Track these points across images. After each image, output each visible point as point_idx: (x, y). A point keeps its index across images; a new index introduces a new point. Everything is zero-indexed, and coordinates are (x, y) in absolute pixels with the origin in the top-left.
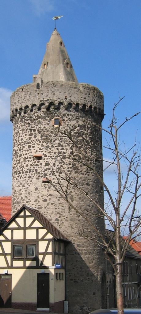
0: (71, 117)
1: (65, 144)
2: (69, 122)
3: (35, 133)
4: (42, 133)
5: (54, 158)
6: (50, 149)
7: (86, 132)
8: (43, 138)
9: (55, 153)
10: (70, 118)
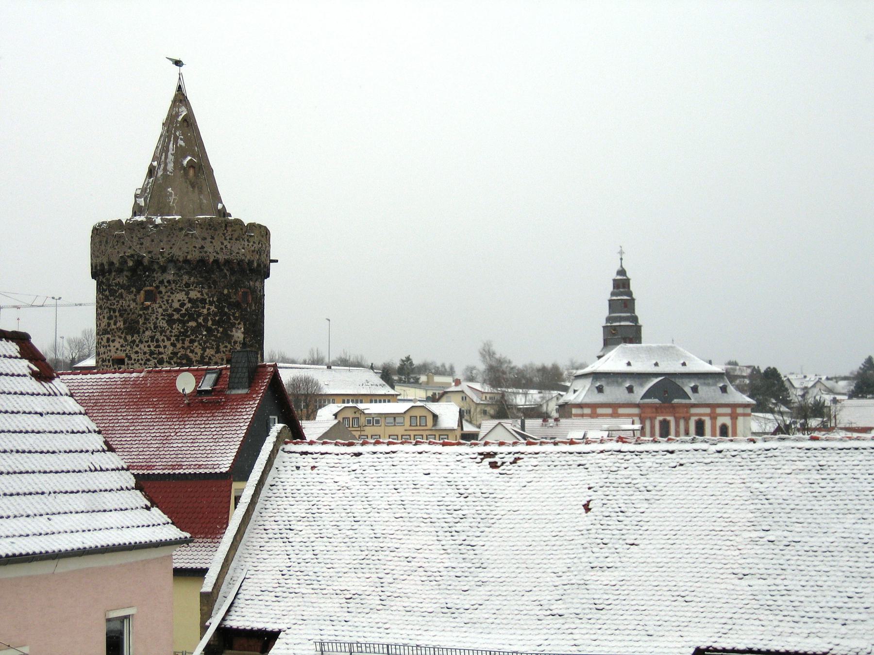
1: (162, 337)
3: (116, 317)
4: (125, 316)
5: (143, 362)
6: (137, 346)
9: (145, 353)
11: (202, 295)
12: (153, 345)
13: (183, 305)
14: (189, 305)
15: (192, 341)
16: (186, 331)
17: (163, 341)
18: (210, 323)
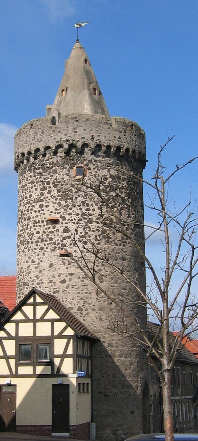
1: (91, 203)
3: (50, 187)
4: (59, 186)
5: (76, 222)
6: (71, 209)
7: (120, 185)
8: (61, 193)
9: (77, 215)
12: (84, 208)
13: (106, 179)
14: (111, 180)
17: (92, 205)
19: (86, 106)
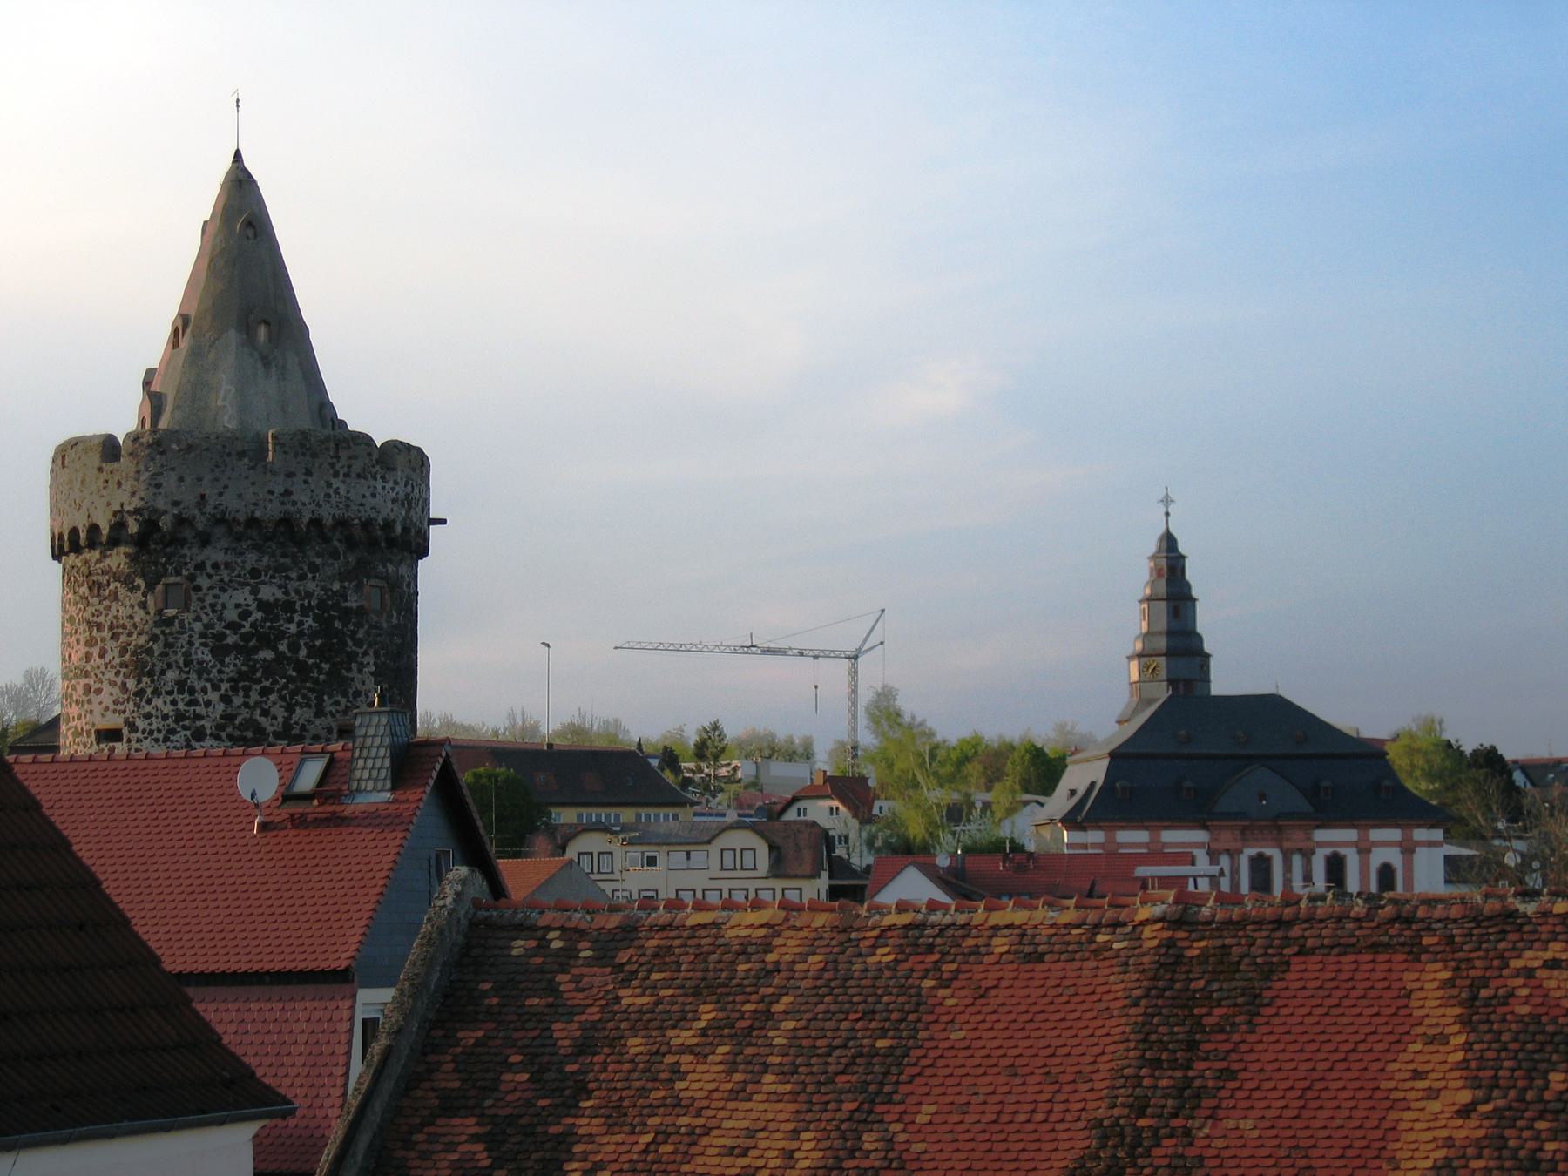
0: (225, 574)
1: (202, 683)
2: (215, 596)
3: (103, 640)
4: (123, 638)
5: (161, 736)
6: (149, 702)
7: (293, 628)
8: (127, 657)
9: (165, 717)
10: (222, 580)
11: (286, 593)
14: (259, 615)
15: (265, 692)
16: (253, 670)
18: (303, 653)
19: (225, 386)
